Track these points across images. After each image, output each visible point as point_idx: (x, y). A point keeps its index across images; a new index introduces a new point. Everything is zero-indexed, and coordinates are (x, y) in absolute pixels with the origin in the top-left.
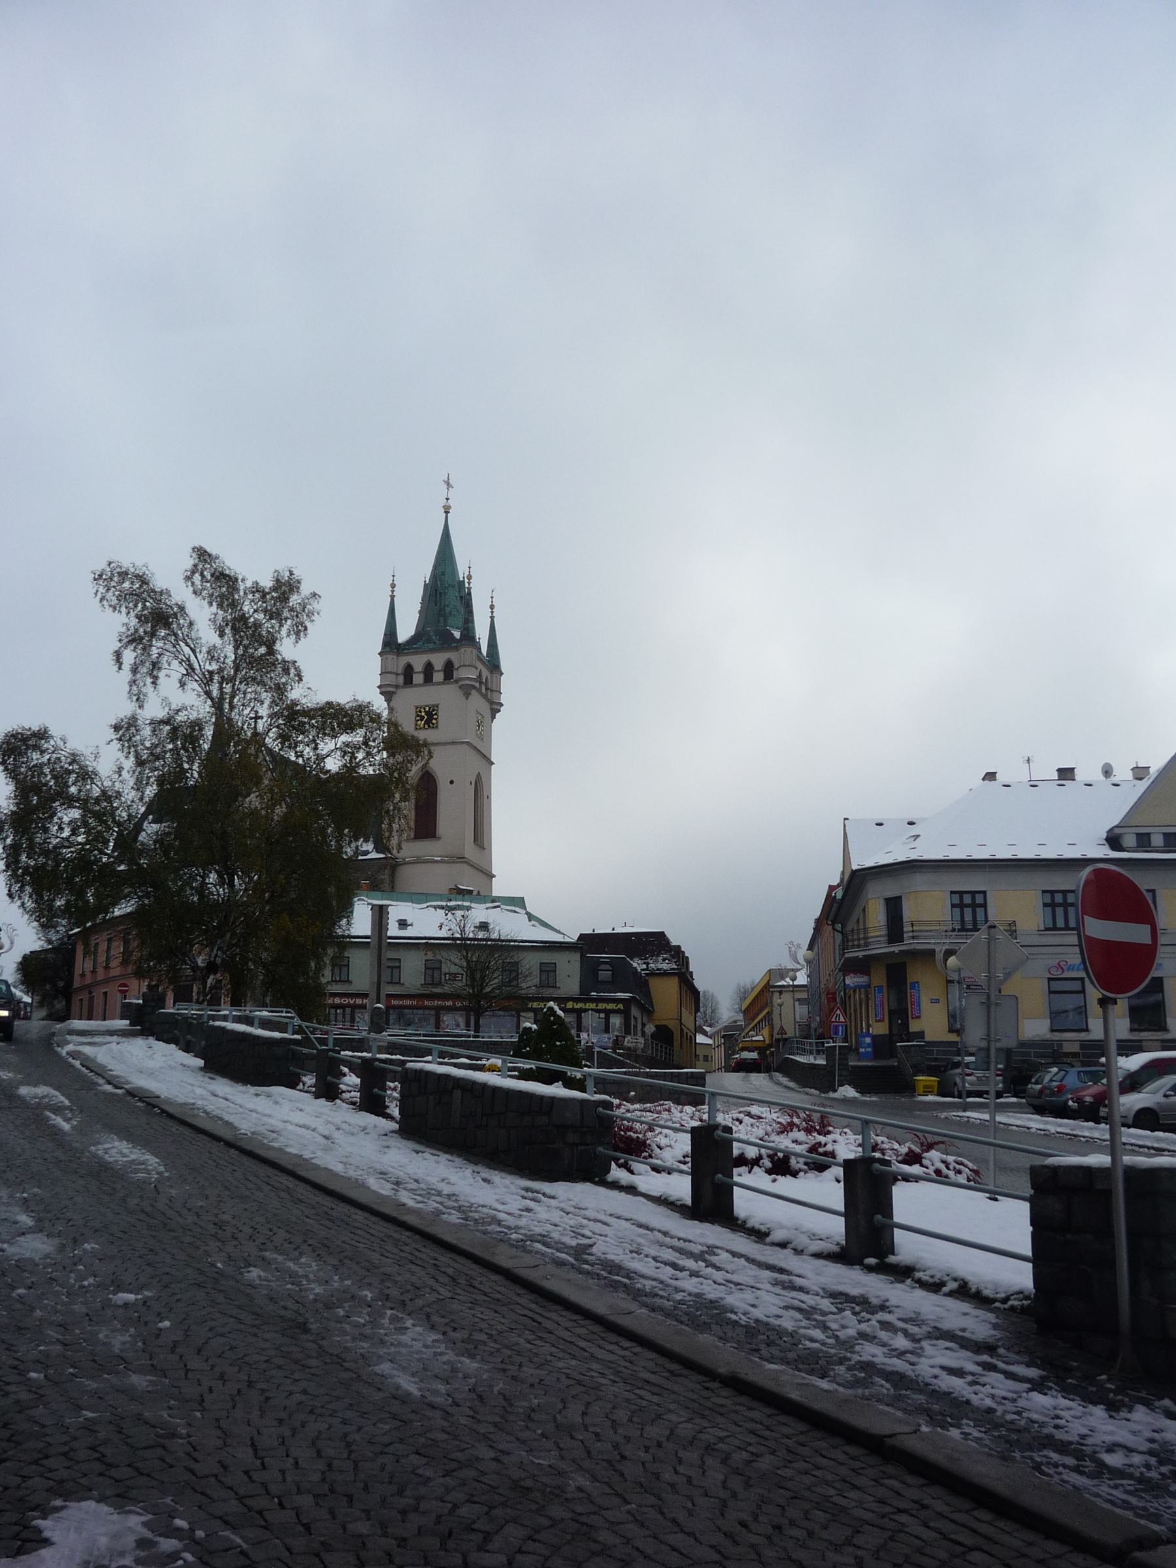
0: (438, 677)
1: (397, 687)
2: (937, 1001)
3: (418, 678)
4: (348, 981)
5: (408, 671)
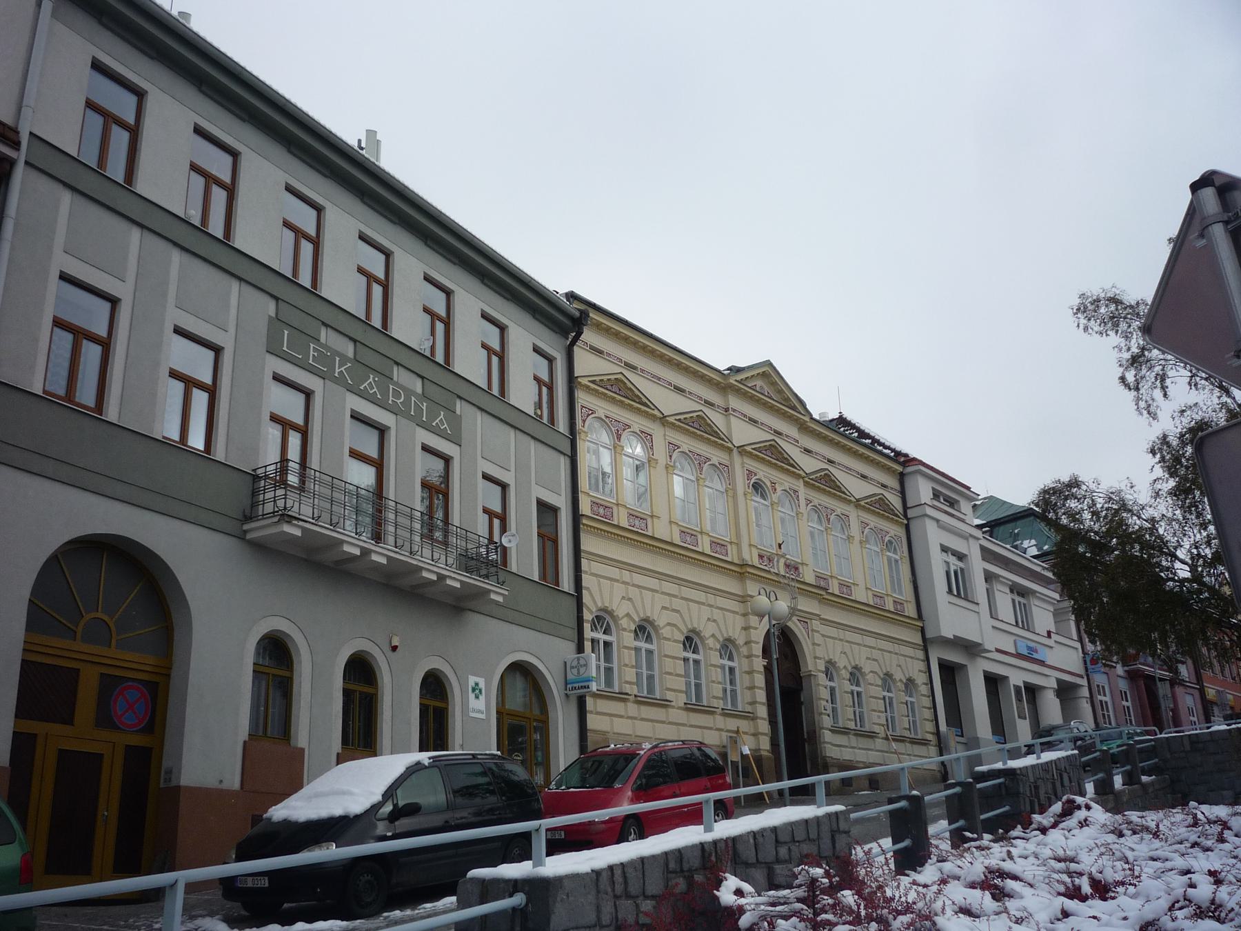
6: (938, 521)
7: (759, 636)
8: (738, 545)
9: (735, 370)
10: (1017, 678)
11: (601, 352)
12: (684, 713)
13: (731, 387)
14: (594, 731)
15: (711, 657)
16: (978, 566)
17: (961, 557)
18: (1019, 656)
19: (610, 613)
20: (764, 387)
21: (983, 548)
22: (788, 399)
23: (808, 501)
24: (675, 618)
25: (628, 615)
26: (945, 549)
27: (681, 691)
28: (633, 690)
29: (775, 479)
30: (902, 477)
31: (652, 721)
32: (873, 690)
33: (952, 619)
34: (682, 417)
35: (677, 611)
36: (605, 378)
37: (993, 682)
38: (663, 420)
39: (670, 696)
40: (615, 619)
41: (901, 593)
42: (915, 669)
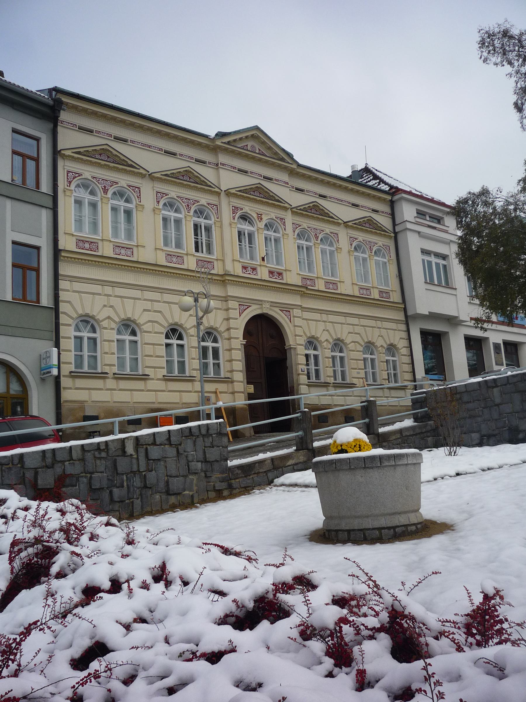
6: (419, 233)
9: (221, 135)
11: (246, 172)
12: (164, 382)
13: (219, 147)
14: (66, 401)
15: (380, 357)
17: (444, 257)
19: (342, 341)
20: (254, 146)
22: (276, 153)
23: (296, 226)
24: (158, 317)
25: (327, 340)
26: (424, 252)
27: (331, 377)
28: (332, 380)
29: (261, 212)
30: (392, 204)
31: (131, 390)
32: (354, 355)
33: (427, 300)
34: (357, 221)
35: (160, 312)
36: (306, 206)
38: (151, 177)
40: (320, 342)
41: (387, 284)
42: (397, 338)
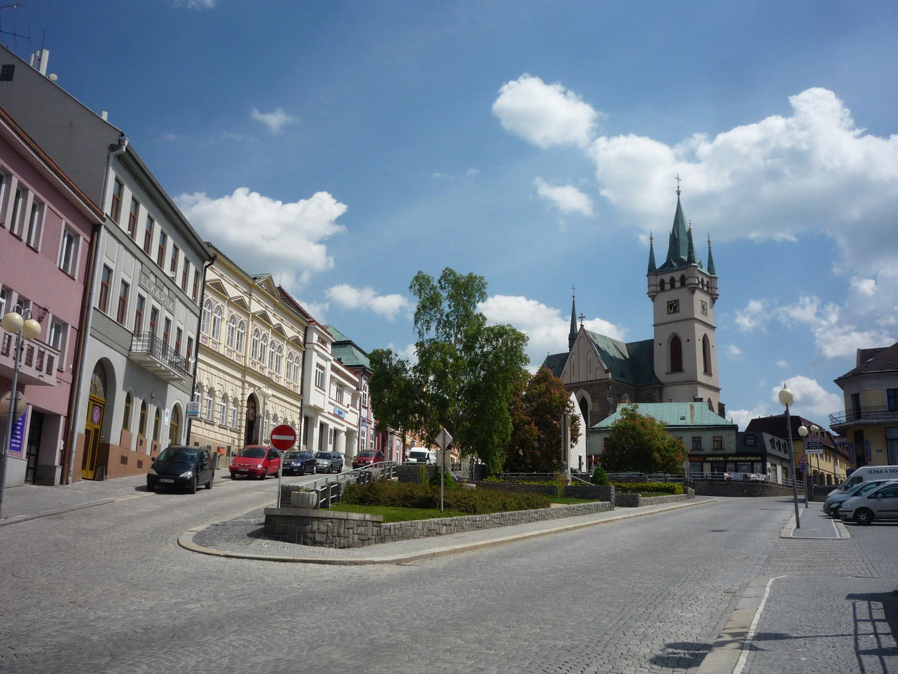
0: (678, 285)
1: (656, 292)
2: (881, 451)
3: (667, 287)
4: (701, 449)
5: (662, 283)
7: (246, 397)
8: (245, 358)
10: (332, 426)
16: (329, 373)
17: (322, 368)
18: (335, 415)
21: (332, 365)
24: (221, 388)
33: (316, 398)
37: (323, 426)
39: (215, 420)
